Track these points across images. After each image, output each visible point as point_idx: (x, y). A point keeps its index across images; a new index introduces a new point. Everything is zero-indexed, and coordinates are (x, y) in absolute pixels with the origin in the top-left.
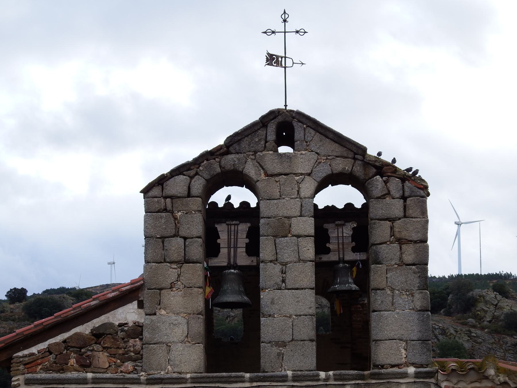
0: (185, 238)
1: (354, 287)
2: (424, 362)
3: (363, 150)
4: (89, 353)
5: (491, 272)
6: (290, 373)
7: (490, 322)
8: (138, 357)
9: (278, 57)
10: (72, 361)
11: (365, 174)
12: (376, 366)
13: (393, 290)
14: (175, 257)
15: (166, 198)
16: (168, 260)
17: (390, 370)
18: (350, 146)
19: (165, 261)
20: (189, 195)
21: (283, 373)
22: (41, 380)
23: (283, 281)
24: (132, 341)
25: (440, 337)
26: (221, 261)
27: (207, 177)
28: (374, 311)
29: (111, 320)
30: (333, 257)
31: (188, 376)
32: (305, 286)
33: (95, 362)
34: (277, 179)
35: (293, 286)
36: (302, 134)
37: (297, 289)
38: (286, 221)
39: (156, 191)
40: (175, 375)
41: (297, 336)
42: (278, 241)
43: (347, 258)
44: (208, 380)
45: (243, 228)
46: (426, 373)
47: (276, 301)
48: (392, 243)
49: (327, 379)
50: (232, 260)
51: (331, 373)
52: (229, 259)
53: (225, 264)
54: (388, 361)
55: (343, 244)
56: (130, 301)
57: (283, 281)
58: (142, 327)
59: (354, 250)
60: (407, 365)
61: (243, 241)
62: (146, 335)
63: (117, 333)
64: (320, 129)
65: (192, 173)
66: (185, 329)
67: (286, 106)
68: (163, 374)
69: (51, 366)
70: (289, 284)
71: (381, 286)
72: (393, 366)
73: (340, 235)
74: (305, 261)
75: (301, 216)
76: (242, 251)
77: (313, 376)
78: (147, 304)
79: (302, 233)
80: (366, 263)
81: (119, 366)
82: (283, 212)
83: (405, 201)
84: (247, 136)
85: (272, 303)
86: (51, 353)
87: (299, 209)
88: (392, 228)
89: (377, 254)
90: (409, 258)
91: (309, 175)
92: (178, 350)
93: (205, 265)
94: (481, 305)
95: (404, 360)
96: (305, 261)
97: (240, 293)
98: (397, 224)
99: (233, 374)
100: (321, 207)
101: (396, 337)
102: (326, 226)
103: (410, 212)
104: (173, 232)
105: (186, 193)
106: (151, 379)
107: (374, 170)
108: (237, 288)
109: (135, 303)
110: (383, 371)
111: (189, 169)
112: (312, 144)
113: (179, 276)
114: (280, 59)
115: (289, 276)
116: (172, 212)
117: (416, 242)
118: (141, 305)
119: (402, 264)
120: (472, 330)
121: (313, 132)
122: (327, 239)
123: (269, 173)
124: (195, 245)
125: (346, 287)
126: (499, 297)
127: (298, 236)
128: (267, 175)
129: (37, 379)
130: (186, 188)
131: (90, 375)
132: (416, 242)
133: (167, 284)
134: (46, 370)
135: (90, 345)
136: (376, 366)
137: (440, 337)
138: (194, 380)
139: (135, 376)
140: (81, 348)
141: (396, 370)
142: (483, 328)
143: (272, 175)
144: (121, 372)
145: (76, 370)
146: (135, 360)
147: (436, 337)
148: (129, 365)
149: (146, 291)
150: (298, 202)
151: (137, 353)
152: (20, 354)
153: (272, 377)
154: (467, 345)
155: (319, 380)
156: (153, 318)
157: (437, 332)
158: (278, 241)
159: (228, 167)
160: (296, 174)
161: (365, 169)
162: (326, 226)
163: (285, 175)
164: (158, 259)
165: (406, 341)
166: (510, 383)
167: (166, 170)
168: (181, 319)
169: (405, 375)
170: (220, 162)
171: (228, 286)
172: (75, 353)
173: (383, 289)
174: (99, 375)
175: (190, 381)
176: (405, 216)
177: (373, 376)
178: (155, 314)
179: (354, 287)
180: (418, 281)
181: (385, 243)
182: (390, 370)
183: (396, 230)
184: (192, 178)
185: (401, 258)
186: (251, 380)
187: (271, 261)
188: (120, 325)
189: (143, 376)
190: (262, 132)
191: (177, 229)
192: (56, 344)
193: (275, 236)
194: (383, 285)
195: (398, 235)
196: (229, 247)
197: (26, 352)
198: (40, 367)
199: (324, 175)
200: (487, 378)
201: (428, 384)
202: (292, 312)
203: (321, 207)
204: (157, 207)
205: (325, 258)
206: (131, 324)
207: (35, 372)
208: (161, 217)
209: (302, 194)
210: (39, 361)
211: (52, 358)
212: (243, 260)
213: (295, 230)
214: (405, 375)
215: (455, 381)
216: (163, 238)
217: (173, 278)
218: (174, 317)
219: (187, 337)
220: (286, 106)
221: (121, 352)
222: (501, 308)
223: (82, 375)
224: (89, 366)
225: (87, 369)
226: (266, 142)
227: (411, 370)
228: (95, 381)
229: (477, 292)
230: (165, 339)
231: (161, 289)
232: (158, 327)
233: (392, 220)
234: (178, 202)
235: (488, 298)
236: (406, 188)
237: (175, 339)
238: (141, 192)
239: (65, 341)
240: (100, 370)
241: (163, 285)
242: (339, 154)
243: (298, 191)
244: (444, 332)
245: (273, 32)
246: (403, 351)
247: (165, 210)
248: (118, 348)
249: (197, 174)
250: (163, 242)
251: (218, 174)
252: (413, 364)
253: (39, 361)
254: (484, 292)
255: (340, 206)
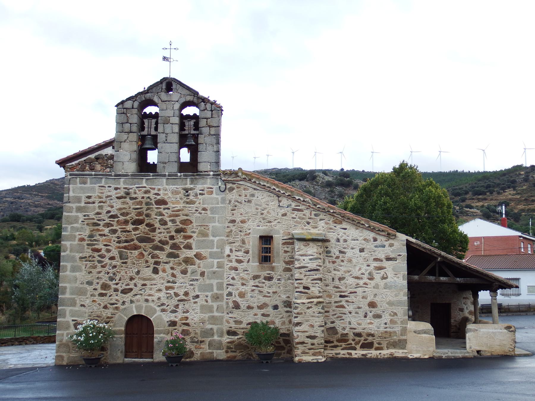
0: (131, 124)
1: (193, 143)
2: (216, 170)
3: (198, 93)
4: (93, 165)
5: (326, 169)
6: (167, 174)
7: (321, 184)
8: (112, 167)
9: (167, 58)
10: (87, 168)
11: (198, 102)
12: (199, 172)
13: (206, 144)
14: (127, 130)
15: (124, 109)
17: (204, 173)
18: (192, 91)
19: (123, 132)
21: (165, 173)
22: (75, 174)
23: (166, 140)
24: (109, 161)
25: (304, 188)
26: (145, 133)
27: (140, 101)
28: (199, 152)
29: (102, 153)
30: (186, 132)
31: (130, 174)
34: (165, 103)
36: (175, 86)
37: (171, 143)
39: (120, 106)
40: (125, 174)
43: (191, 133)
45: (154, 121)
46: (217, 174)
47: (163, 147)
48: (206, 127)
49: (181, 176)
50: (149, 133)
51: (182, 174)
52: (148, 132)
53: (147, 134)
54: (203, 170)
57: (166, 140)
58: (113, 156)
59: (194, 130)
60: (210, 171)
61: (153, 126)
62: (115, 158)
63: (104, 158)
64: (182, 85)
65: (134, 100)
66: (130, 157)
68: (120, 173)
69: (79, 169)
71: (202, 143)
72: (205, 172)
73: (189, 124)
75: (173, 116)
76: (153, 129)
77: (176, 175)
78: (115, 148)
80: (198, 134)
81: (105, 170)
82: (167, 115)
83: (212, 112)
84: (155, 87)
85: (162, 148)
86: (80, 165)
87: (173, 114)
88: (207, 122)
89: (201, 131)
90: (212, 132)
91: (177, 101)
92: (126, 164)
93: (139, 134)
94: (318, 178)
95: (209, 170)
97: (151, 144)
98: (209, 120)
99: (143, 173)
100: (184, 114)
102: (184, 121)
103: (213, 116)
104: (126, 121)
105: (132, 107)
106: (116, 175)
107: (201, 100)
108: (150, 143)
110: (201, 173)
111: (133, 99)
112: (179, 90)
113: (128, 137)
114: (168, 59)
115: (168, 138)
116: (126, 114)
117: (215, 127)
118: (113, 148)
119: (210, 134)
120: (315, 186)
121: (179, 86)
122: (185, 126)
123: (162, 100)
124: (134, 126)
125: (190, 143)
126: (324, 175)
127: (172, 124)
128: (162, 101)
129: (74, 174)
130: (132, 105)
131: (93, 173)
132: (215, 127)
133: (123, 140)
134: (78, 171)
135: (94, 162)
136: (199, 172)
137: (304, 188)
138: (132, 175)
139: (110, 173)
140: (91, 163)
141: (206, 173)
142: (318, 186)
143: (164, 101)
144: (105, 172)
145: (88, 171)
147: (303, 188)
148: (108, 170)
149: (115, 143)
150: (173, 111)
151: (111, 165)
152: (68, 165)
153: (160, 175)
154: (313, 191)
155: (178, 176)
156: (118, 152)
157: (303, 187)
158: (165, 125)
159: (148, 98)
161: (198, 100)
162: (184, 121)
163: (168, 101)
164: (120, 131)
166: (247, 178)
167: (124, 99)
168: (128, 154)
169: (209, 175)
170: (144, 96)
171: (147, 142)
172: (88, 164)
173: (203, 144)
174: (96, 173)
175: (130, 175)
176: (212, 117)
177: (197, 175)
178: (118, 151)
179: (193, 143)
180: (215, 141)
181: (204, 127)
182: (204, 173)
184: (134, 101)
186: (153, 176)
187: (162, 133)
188: (105, 155)
189: (113, 174)
190: (160, 85)
191: (128, 120)
192: (82, 161)
195: (209, 124)
196: (148, 128)
197: (70, 164)
198: (75, 169)
199: (183, 102)
200: (238, 176)
201: (218, 178)
202: (169, 151)
203: (184, 114)
204: (121, 112)
205: (184, 133)
206: (109, 155)
207: (74, 171)
209: (174, 109)
210: (75, 167)
211: (80, 166)
212: (153, 132)
213: (171, 122)
214: (209, 175)
215: (227, 177)
216: (122, 123)
217: (126, 138)
218: (125, 152)
219: (130, 160)
221: (105, 164)
222: (325, 179)
223: (90, 173)
224: (93, 169)
225: (93, 171)
226: (162, 89)
227: (212, 173)
228: (95, 175)
229: (317, 174)
230: (122, 160)
231: (121, 142)
232: (119, 156)
233: (207, 119)
234: (128, 110)
235: (320, 176)
236: (213, 107)
237: (125, 161)
238: (115, 106)
239: (85, 160)
240: (97, 171)
241: (122, 141)
242: (188, 94)
243: (173, 107)
244: (305, 187)
245: (166, 49)
246: (209, 166)
247: (124, 113)
249: (136, 100)
250: (122, 125)
251: (144, 100)
253: (75, 167)
254: (319, 174)
255: (192, 114)
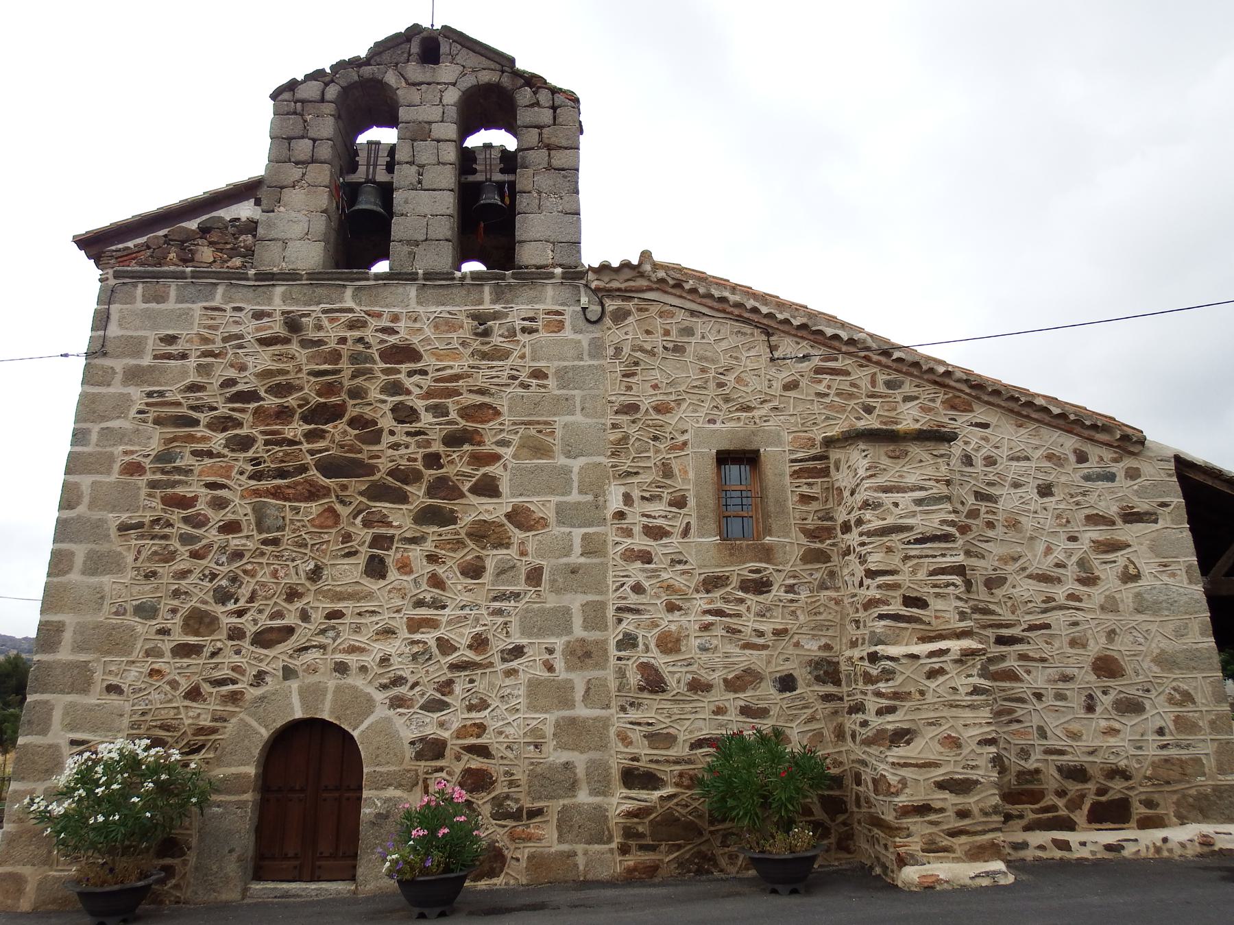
0: (314, 140)
3: (512, 61)
8: (250, 253)
10: (172, 255)
13: (539, 193)
14: (302, 157)
16: (293, 160)
20: (323, 100)
23: (420, 182)
26: (360, 176)
28: (519, 213)
32: (443, 187)
33: (198, 257)
35: (430, 187)
36: (448, 48)
37: (434, 190)
38: (427, 126)
39: (286, 95)
41: (432, 235)
42: (415, 144)
44: (326, 276)
48: (539, 148)
52: (368, 175)
55: (491, 165)
56: (247, 199)
59: (502, 171)
62: (261, 231)
63: (226, 228)
66: (306, 226)
67: (432, 25)
70: (426, 185)
71: (527, 189)
73: (488, 156)
74: (444, 164)
78: (264, 202)
79: (443, 137)
85: (406, 202)
88: (540, 134)
96: (444, 164)
97: (376, 204)
98: (545, 131)
101: (542, 238)
109: (252, 201)
113: (304, 174)
116: (302, 115)
127: (438, 141)
143: (414, 84)
146: (244, 257)
150: (440, 109)
152: (113, 248)
158: (415, 144)
159: (367, 75)
160: (438, 84)
164: (282, 158)
165: (553, 243)
168: (300, 216)
173: (529, 192)
175: (305, 276)
178: (273, 211)
181: (533, 149)
183: (545, 136)
184: (326, 85)
185: (549, 163)
187: (407, 163)
193: (414, 140)
194: (529, 187)
195: (546, 141)
196: (368, 165)
199: (470, 85)
202: (427, 211)
205: (471, 178)
208: (289, 119)
209: (445, 102)
211: (149, 252)
212: (382, 176)
213: (435, 134)
216: (289, 139)
218: (294, 214)
219: (307, 234)
220: (432, 25)
224: (192, 260)
227: (558, 271)
230: (281, 235)
237: (293, 236)
241: (285, 183)
243: (441, 99)
246: (551, 253)
247: (295, 113)
248: (226, 243)
252: (560, 265)
